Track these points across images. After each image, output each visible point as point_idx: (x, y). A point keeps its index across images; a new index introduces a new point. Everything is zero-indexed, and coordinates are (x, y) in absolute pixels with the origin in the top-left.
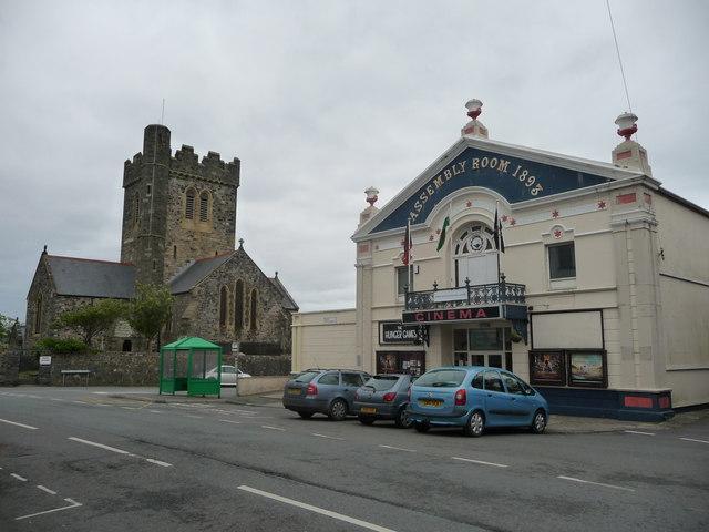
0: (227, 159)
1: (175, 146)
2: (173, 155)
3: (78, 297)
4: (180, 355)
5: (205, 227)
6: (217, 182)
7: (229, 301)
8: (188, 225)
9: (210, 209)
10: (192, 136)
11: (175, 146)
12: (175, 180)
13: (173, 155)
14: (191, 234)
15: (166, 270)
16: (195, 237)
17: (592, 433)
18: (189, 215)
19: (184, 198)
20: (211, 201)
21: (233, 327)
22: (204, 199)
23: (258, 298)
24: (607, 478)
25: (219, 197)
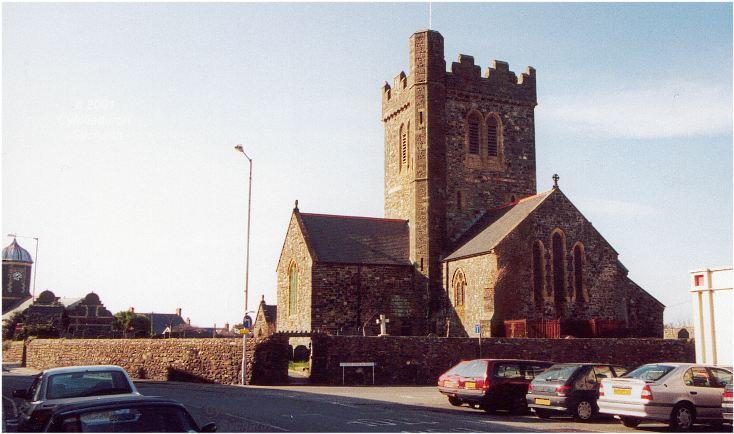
0: (519, 70)
1: (451, 57)
2: (449, 69)
3: (343, 265)
4: (10, 290)
5: (495, 164)
6: (506, 102)
7: (544, 262)
8: (472, 162)
9: (501, 139)
10: (478, 45)
11: (451, 57)
12: (453, 103)
13: (449, 69)
14: (479, 174)
15: (450, 225)
16: (484, 178)
17: (706, 407)
18: (474, 149)
19: (464, 124)
20: (501, 128)
21: (552, 299)
22: (492, 129)
23: (584, 258)
24: (356, 405)
25: (512, 121)
